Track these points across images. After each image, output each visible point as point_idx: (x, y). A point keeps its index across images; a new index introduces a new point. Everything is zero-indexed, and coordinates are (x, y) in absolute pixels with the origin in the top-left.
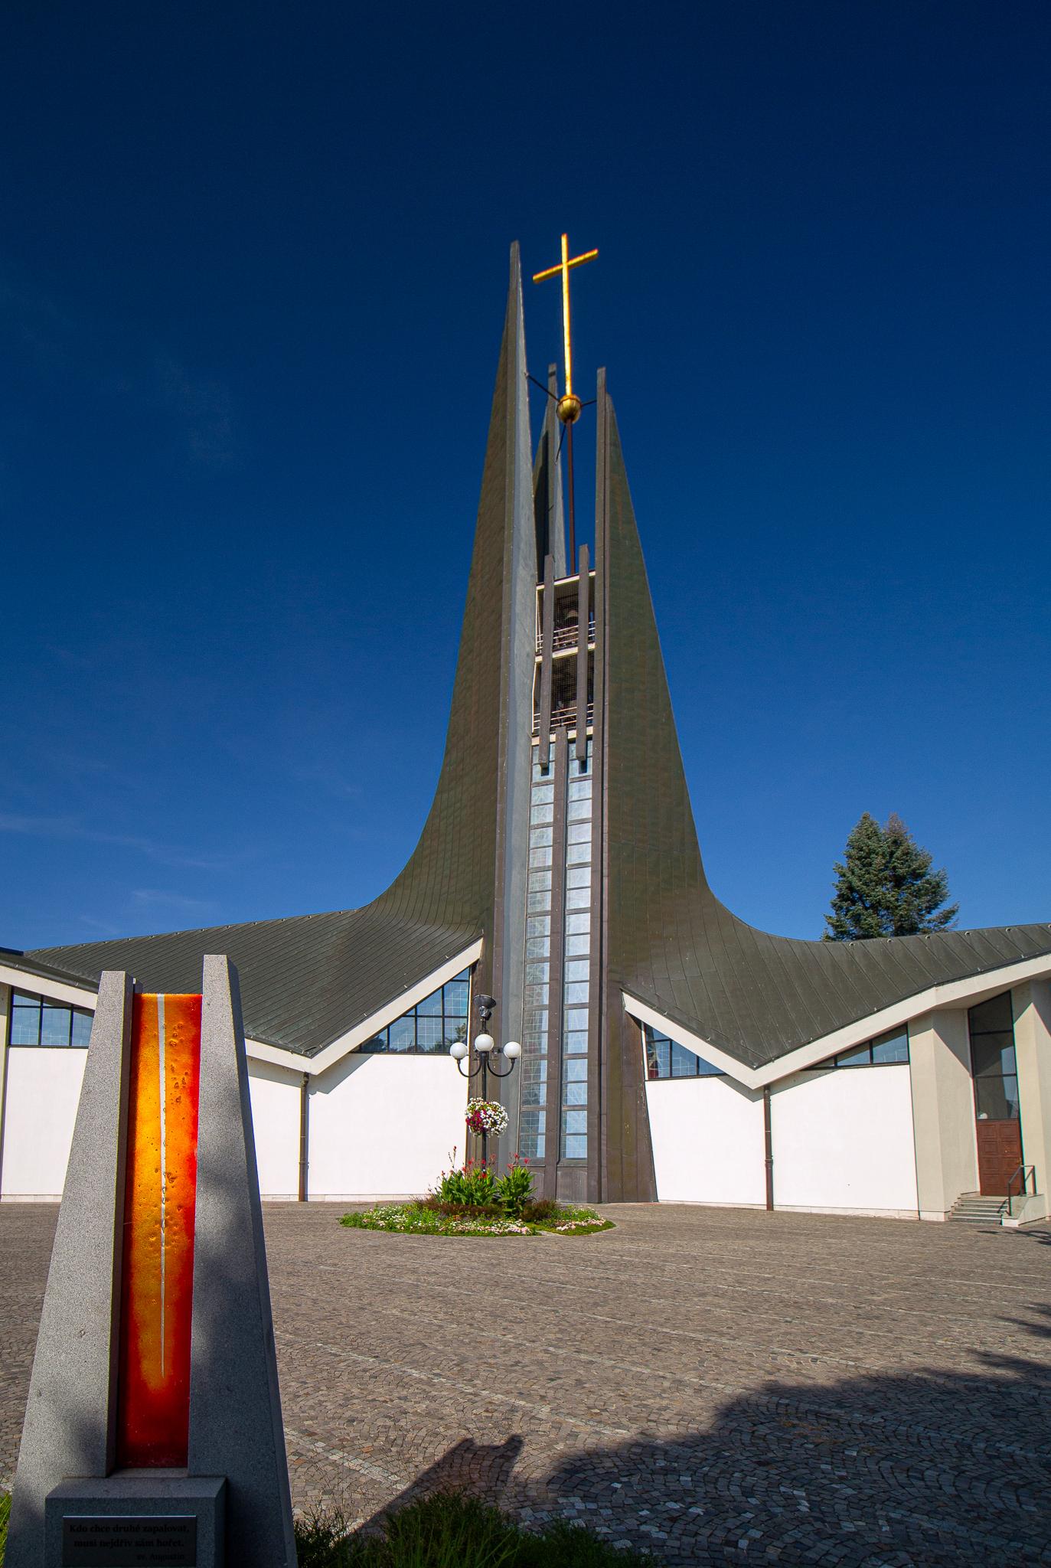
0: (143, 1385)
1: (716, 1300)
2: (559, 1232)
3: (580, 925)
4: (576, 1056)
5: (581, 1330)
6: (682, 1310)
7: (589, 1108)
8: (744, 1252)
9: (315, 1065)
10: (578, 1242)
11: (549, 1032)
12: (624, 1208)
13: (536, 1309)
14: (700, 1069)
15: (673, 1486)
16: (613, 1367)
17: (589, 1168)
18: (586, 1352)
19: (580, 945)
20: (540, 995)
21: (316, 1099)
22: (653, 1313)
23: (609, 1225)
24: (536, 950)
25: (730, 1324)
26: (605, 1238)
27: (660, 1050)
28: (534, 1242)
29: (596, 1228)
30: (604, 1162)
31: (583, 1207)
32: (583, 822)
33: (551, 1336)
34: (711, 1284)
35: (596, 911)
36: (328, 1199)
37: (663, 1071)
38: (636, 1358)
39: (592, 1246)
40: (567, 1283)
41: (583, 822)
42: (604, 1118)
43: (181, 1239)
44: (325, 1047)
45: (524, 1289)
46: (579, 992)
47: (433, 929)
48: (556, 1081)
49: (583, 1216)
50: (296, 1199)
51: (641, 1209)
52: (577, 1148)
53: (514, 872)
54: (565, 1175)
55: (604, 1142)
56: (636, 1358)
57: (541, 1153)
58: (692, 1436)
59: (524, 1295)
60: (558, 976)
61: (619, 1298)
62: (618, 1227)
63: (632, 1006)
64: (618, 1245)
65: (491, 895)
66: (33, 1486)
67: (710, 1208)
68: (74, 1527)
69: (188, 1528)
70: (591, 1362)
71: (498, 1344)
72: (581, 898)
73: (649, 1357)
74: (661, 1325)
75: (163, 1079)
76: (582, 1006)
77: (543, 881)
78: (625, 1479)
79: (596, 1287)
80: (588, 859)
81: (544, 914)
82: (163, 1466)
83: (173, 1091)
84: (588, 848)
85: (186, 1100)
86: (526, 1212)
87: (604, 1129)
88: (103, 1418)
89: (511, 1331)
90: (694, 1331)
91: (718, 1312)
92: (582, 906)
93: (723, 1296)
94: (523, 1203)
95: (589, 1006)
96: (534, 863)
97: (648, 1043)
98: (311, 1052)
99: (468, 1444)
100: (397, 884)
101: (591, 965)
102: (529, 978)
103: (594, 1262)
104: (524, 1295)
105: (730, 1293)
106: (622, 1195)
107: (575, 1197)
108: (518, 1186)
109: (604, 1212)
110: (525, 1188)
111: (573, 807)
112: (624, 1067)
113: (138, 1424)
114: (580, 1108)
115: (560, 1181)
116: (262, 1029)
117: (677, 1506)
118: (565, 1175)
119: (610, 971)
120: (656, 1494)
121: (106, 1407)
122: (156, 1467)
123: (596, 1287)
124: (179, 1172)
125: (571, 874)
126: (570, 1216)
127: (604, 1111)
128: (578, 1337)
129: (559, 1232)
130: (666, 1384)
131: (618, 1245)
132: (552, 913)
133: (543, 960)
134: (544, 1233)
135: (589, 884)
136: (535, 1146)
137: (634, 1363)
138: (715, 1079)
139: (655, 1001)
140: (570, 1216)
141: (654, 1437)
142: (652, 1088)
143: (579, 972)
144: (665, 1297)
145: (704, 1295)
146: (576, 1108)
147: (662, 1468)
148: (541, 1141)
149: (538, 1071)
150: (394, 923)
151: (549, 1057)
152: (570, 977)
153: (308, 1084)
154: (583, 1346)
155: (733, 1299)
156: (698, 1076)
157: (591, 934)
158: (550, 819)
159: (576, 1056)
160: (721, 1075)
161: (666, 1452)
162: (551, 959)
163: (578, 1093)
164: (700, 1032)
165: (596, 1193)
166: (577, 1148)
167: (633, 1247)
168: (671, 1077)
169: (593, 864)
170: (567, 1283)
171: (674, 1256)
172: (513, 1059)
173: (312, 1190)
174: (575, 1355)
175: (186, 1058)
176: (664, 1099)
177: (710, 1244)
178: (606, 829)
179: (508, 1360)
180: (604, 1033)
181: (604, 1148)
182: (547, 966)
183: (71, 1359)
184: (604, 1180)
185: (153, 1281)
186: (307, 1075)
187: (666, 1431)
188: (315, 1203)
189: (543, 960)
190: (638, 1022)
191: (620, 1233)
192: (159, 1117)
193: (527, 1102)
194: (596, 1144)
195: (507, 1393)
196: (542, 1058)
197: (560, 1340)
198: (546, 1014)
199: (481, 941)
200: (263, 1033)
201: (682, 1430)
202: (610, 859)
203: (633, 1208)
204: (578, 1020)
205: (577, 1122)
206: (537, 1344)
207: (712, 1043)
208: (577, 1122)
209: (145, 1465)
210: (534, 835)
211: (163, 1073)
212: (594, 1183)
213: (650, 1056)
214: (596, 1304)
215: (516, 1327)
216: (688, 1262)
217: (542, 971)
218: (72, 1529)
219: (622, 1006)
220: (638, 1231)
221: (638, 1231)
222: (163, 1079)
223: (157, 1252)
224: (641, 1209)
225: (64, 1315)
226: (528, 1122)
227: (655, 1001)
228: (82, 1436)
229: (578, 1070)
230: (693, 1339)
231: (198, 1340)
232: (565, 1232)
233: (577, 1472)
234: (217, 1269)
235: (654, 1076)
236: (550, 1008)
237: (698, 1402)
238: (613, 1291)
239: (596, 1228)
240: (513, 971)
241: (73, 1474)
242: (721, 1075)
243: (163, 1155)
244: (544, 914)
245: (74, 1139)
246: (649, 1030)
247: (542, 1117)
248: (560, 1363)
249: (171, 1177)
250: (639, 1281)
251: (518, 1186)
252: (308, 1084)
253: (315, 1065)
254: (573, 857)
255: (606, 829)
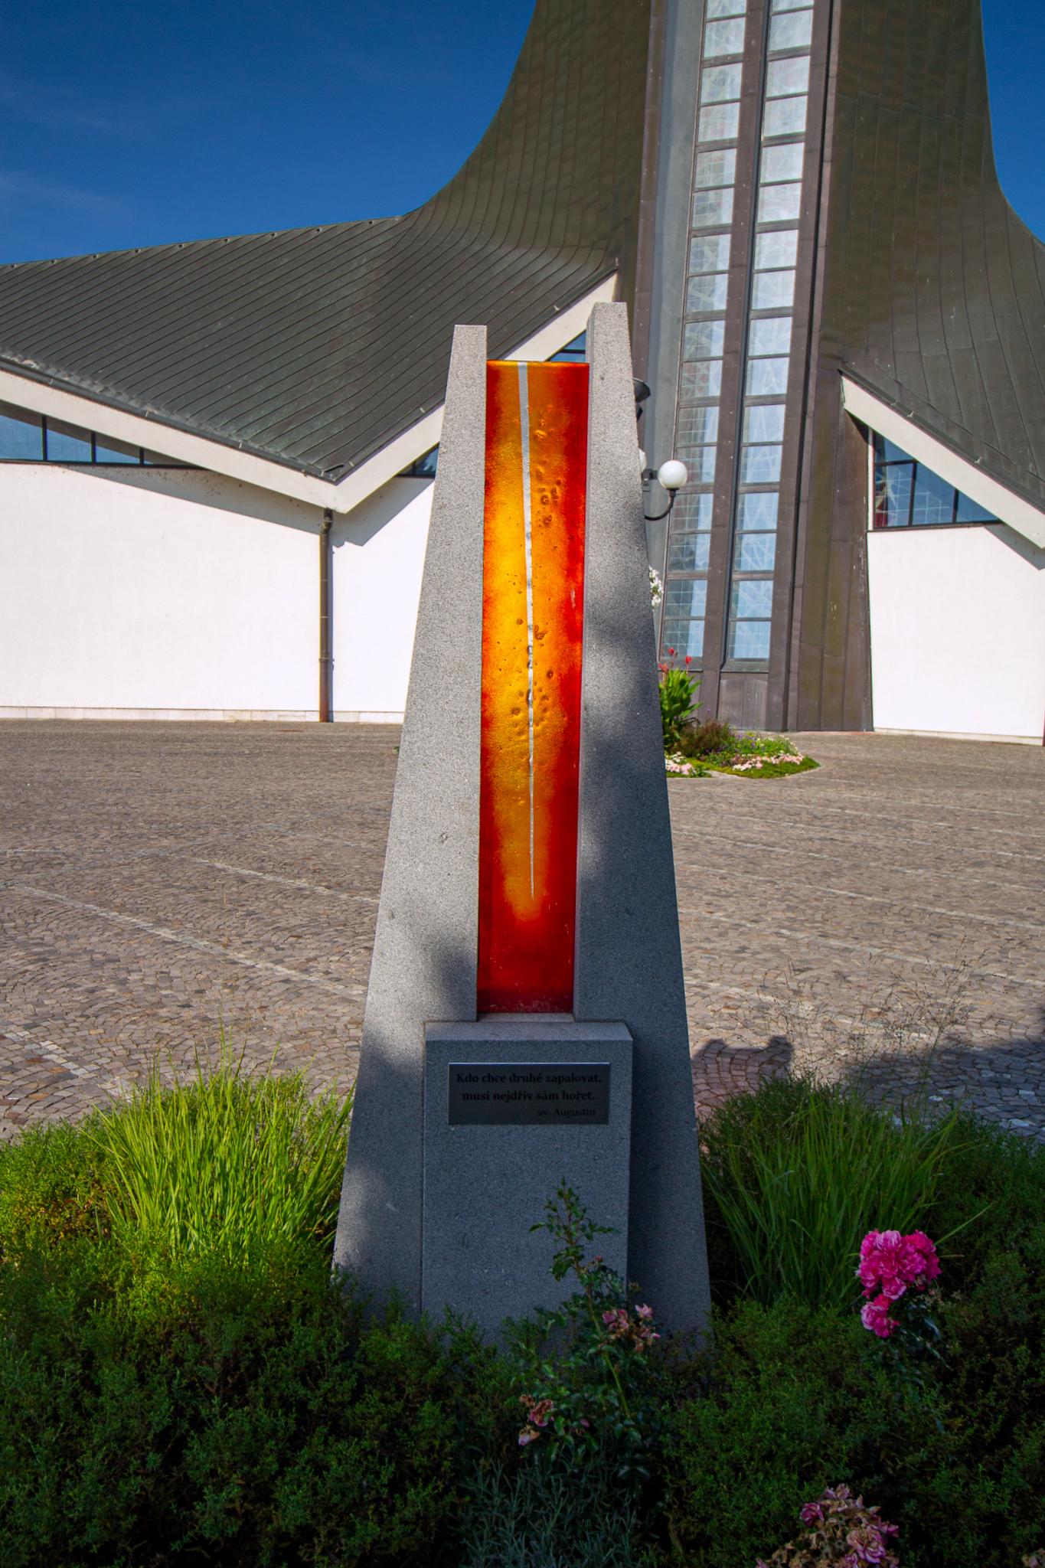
0: (507, 908)
1: (1000, 872)
2: (738, 773)
3: (779, 251)
4: (759, 488)
5: (817, 909)
6: (954, 884)
7: (776, 576)
8: (1025, 806)
9: (343, 497)
10: (770, 788)
11: (719, 445)
12: (822, 740)
13: (746, 879)
14: (959, 512)
15: (1014, 1102)
16: (881, 957)
17: (771, 674)
18: (836, 937)
19: (776, 289)
20: (705, 378)
21: (345, 555)
22: (915, 887)
23: (809, 764)
24: (703, 297)
25: (1030, 904)
26: (810, 783)
27: (894, 478)
28: (702, 785)
29: (792, 768)
30: (794, 665)
31: (771, 737)
32: (793, 53)
33: (779, 915)
34: (988, 849)
35: (808, 227)
36: (365, 719)
37: (895, 516)
38: (908, 945)
39: (796, 793)
40: (774, 845)
41: (793, 53)
42: (798, 592)
43: (554, 718)
44: (358, 465)
45: (714, 852)
46: (771, 376)
47: (531, 256)
48: (727, 530)
49: (771, 749)
50: (316, 718)
51: (849, 741)
52: (752, 642)
53: (674, 152)
54: (733, 686)
55: (796, 633)
56: (908, 945)
57: (695, 648)
58: (1020, 1043)
59: (720, 861)
60: (738, 345)
61: (856, 866)
62: (823, 767)
63: (857, 401)
64: (831, 793)
65: (634, 194)
66: (387, 1033)
67: (954, 742)
68: (460, 1076)
69: (599, 1076)
70: (846, 949)
71: (706, 924)
72: (782, 203)
73: (927, 945)
74: (931, 904)
75: (527, 491)
76: (773, 400)
77: (719, 169)
78: (946, 1092)
79: (819, 851)
80: (800, 126)
81: (719, 230)
82: (535, 1011)
83: (539, 507)
84: (801, 105)
85: (557, 522)
86: (684, 742)
87: (797, 611)
88: (472, 946)
89: (719, 908)
90: (982, 912)
91: (1007, 887)
92: (785, 216)
93: (1009, 865)
94: (680, 728)
95: (787, 400)
96: (706, 135)
97: (879, 468)
98: (335, 473)
99: (717, 1047)
100: (471, 169)
101: (795, 327)
102: (689, 350)
103: (805, 816)
104: (720, 861)
105: (1018, 862)
106: (817, 721)
107: (747, 721)
108: (673, 700)
109: (800, 744)
110: (685, 704)
111: (778, 24)
112: (838, 498)
113: (516, 958)
114: (762, 575)
115: (725, 695)
116: (252, 432)
117: (1026, 1124)
118: (733, 686)
119: (824, 338)
120: (992, 1109)
121: (476, 933)
122: (526, 1011)
123: (819, 851)
124: (552, 629)
125: (769, 154)
126: (751, 749)
127: (799, 581)
128: (818, 917)
129: (738, 773)
130: (962, 979)
131: (831, 793)
132: (734, 229)
133: (713, 316)
134: (714, 773)
135: (798, 174)
136: (685, 637)
137: (908, 952)
138: (981, 532)
139: (894, 392)
140: (751, 749)
141: (970, 1044)
142: (881, 547)
143: (773, 338)
144: (921, 866)
145: (979, 864)
146: (754, 576)
147: (991, 1080)
148: (697, 632)
149: (697, 512)
150: (463, 244)
151: (717, 489)
152: (756, 348)
153: (331, 528)
154: (828, 928)
155: (1024, 870)
156: (955, 524)
157: (798, 268)
158: (737, 46)
159: (759, 488)
160: (992, 523)
161: (991, 1062)
162: (727, 315)
163: (759, 551)
164: (965, 450)
165: (780, 716)
166: (752, 642)
167: (856, 796)
168: (910, 526)
169: (807, 137)
170: (774, 845)
171: (921, 809)
172: (673, 491)
173: (338, 704)
174: (822, 939)
175: (557, 460)
176: (900, 567)
177: (970, 794)
178: (834, 69)
179: (734, 941)
180: (807, 448)
181: (795, 642)
182: (719, 328)
183: (430, 878)
184: (793, 695)
185: (520, 773)
186: (329, 513)
187: (980, 1036)
188: (340, 724)
189: (713, 316)
190: (863, 428)
191: (830, 775)
192: (522, 545)
193: (677, 565)
194: (785, 636)
195: (746, 986)
196: (705, 489)
197: (794, 920)
198: (714, 414)
199: (612, 281)
200: (254, 439)
201: (1005, 1036)
202: (839, 126)
203: (837, 740)
204: (767, 425)
205: (755, 599)
206: (762, 925)
207: (984, 468)
208: (755, 599)
209: (512, 1009)
210: (710, 76)
211: (527, 482)
212: (777, 699)
213: (879, 488)
214: (826, 874)
215: (723, 901)
216: (943, 819)
217: (710, 336)
218: (459, 1078)
219: (838, 399)
220: (856, 774)
221: (856, 774)
222: (527, 491)
223: (529, 735)
224: (849, 741)
225: (421, 814)
226: (677, 599)
227: (894, 392)
228: (445, 968)
229: (761, 512)
230: (982, 923)
231: (587, 848)
232: (747, 774)
233: (878, 1082)
234: (610, 753)
235: (882, 524)
236: (722, 402)
237: (1014, 1002)
238: (846, 857)
239: (792, 768)
240: (664, 336)
241: (436, 1017)
242: (992, 523)
243: (530, 599)
244: (719, 230)
245: (426, 574)
246: (879, 442)
247: (700, 593)
248: (803, 949)
249: (538, 636)
250: (880, 844)
251: (673, 700)
252: (331, 528)
253: (343, 497)
254: (773, 126)
255: (834, 69)
